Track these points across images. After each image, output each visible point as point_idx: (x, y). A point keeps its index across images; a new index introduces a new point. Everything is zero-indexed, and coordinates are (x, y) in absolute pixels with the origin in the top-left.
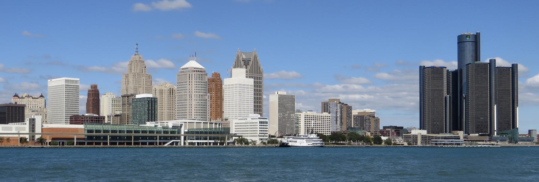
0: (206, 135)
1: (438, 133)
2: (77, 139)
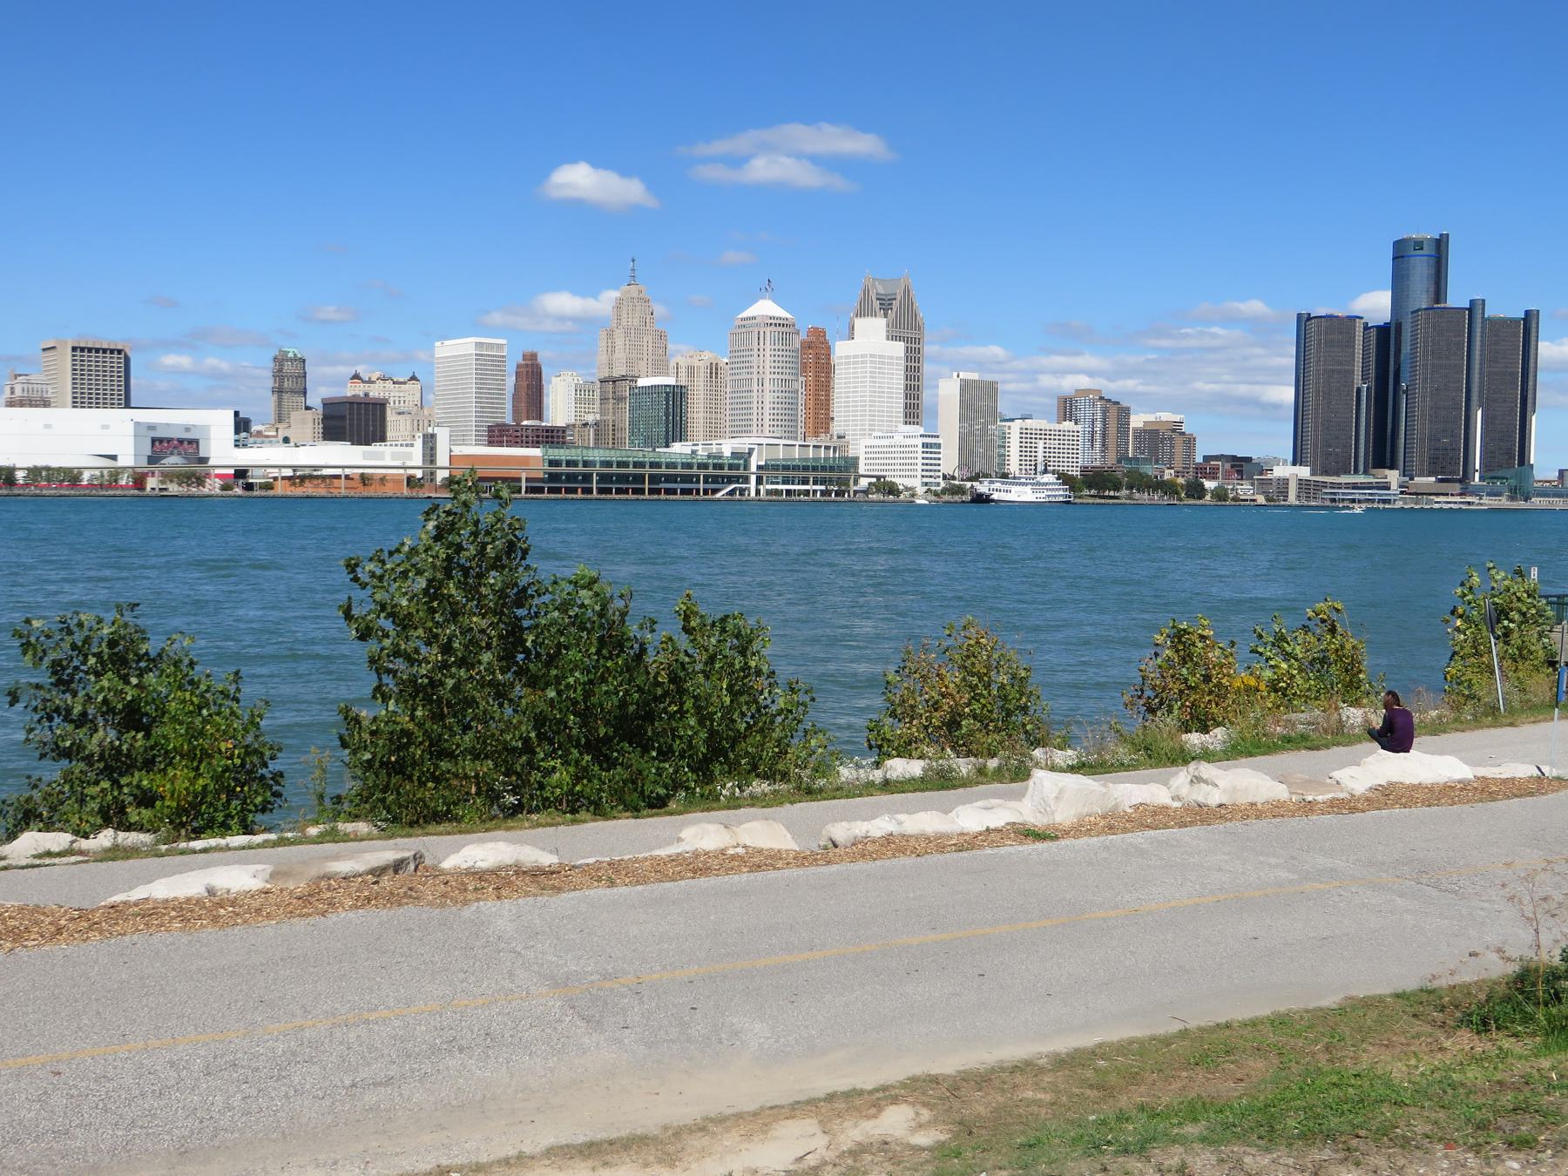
0: (805, 474)
1: (1338, 474)
2: (528, 480)
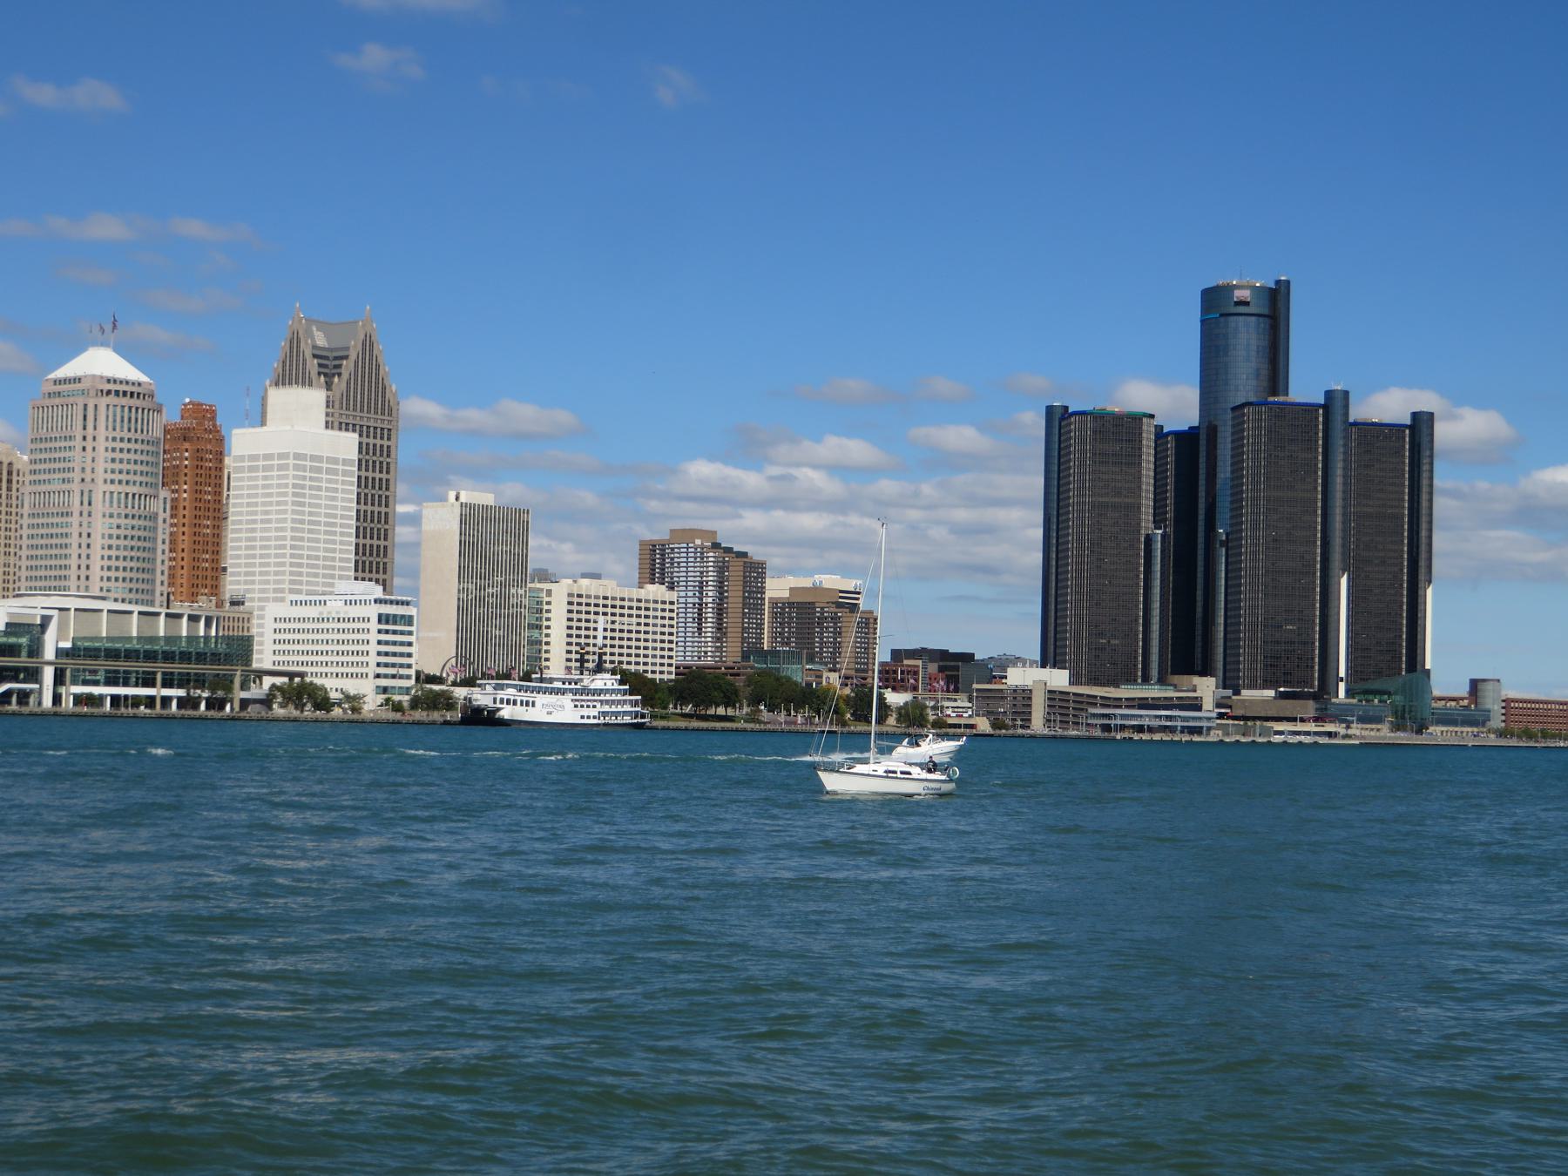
1: (1115, 684)
